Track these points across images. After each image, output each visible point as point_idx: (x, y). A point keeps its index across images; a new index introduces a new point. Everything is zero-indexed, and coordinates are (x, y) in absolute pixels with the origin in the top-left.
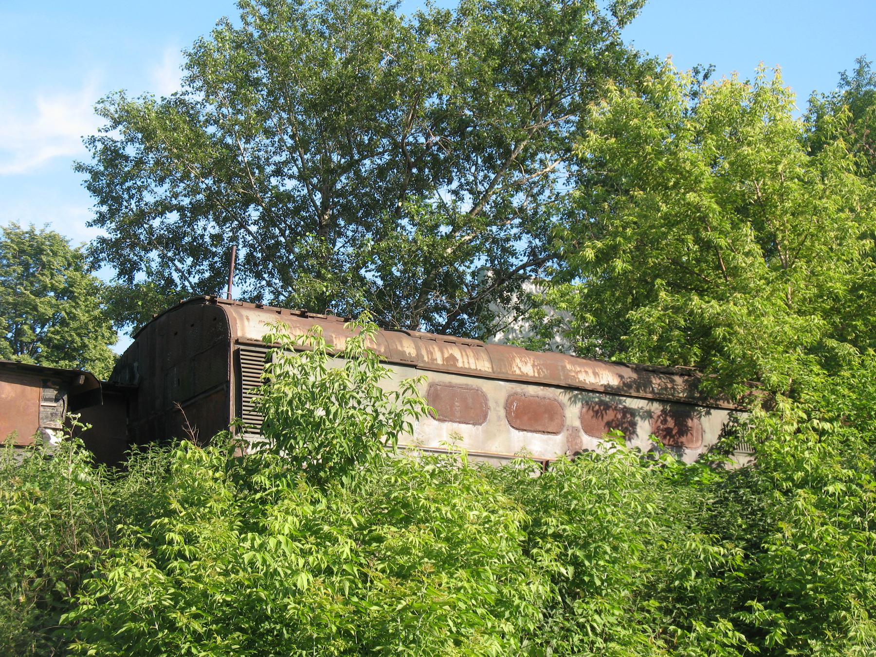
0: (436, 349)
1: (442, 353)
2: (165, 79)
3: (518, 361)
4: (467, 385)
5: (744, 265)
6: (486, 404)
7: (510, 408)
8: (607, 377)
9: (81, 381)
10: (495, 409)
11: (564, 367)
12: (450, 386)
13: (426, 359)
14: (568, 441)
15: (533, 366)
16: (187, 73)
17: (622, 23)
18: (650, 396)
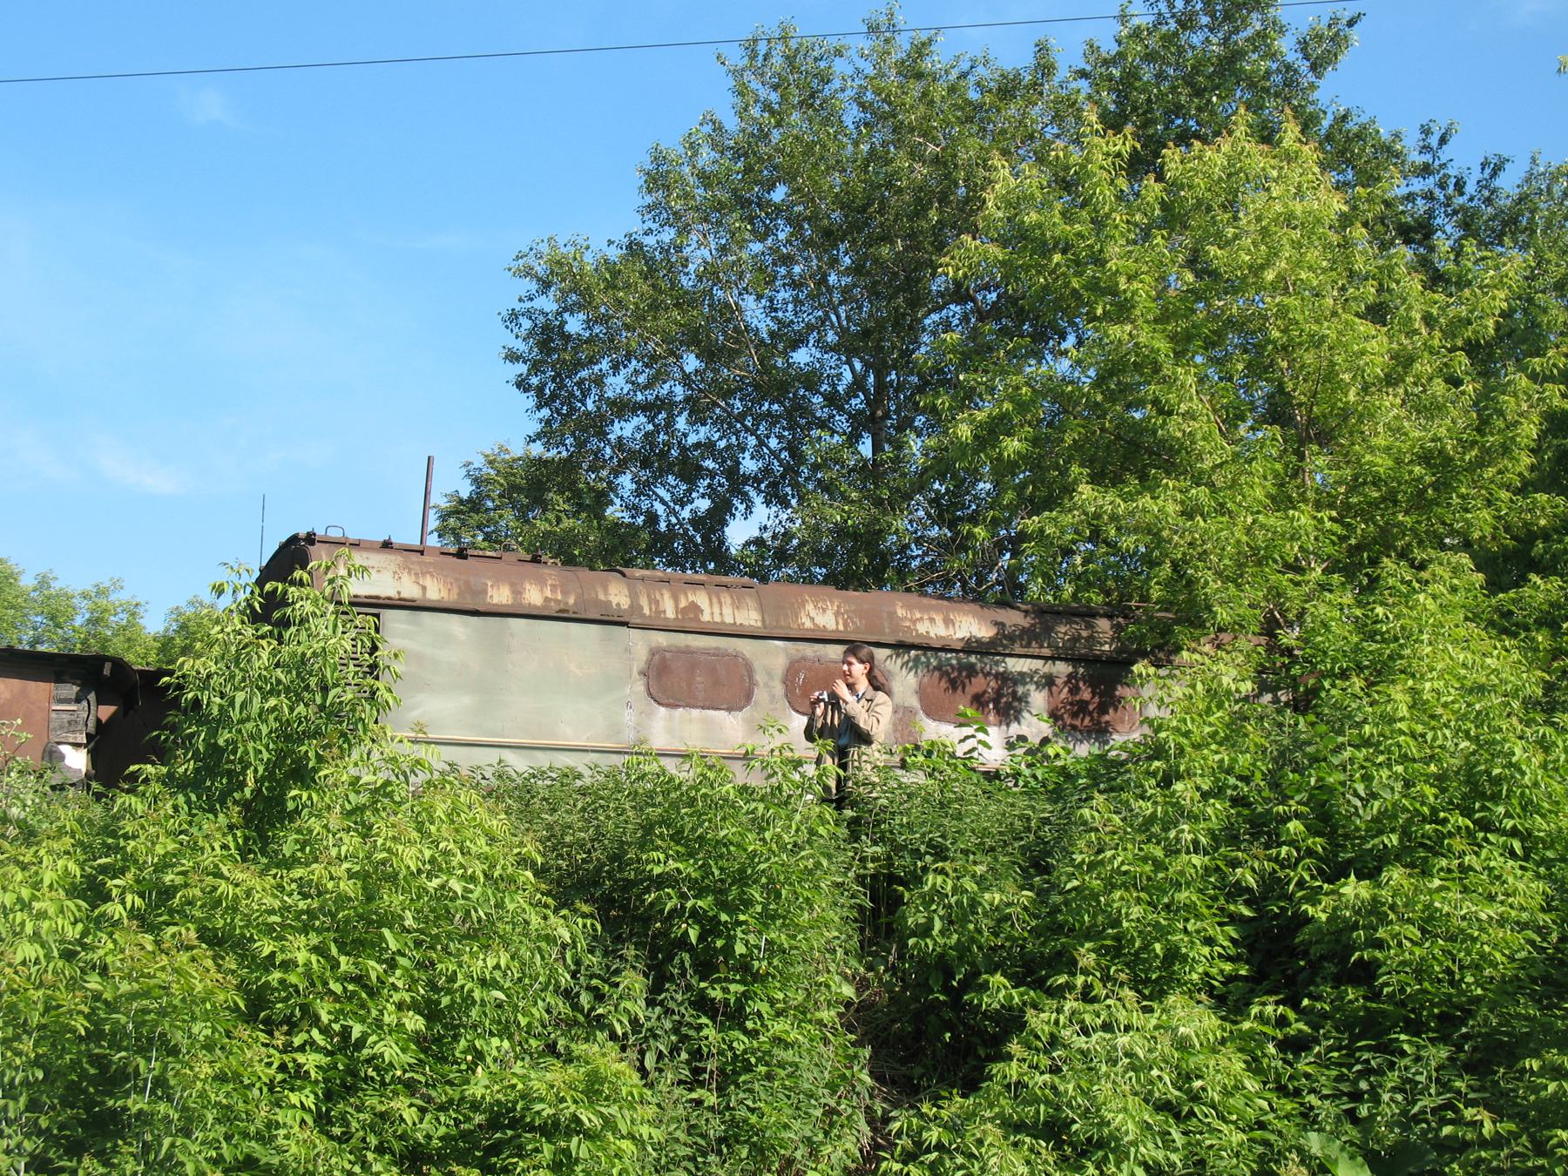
0: (667, 595)
1: (676, 601)
2: (605, 220)
3: (810, 607)
4: (717, 649)
5: (1179, 435)
6: (751, 678)
7: (793, 682)
8: (970, 625)
9: (107, 671)
10: (766, 685)
11: (892, 614)
12: (688, 651)
13: (646, 611)
14: (895, 730)
15: (837, 614)
16: (649, 200)
17: (1317, 67)
18: (1046, 652)
